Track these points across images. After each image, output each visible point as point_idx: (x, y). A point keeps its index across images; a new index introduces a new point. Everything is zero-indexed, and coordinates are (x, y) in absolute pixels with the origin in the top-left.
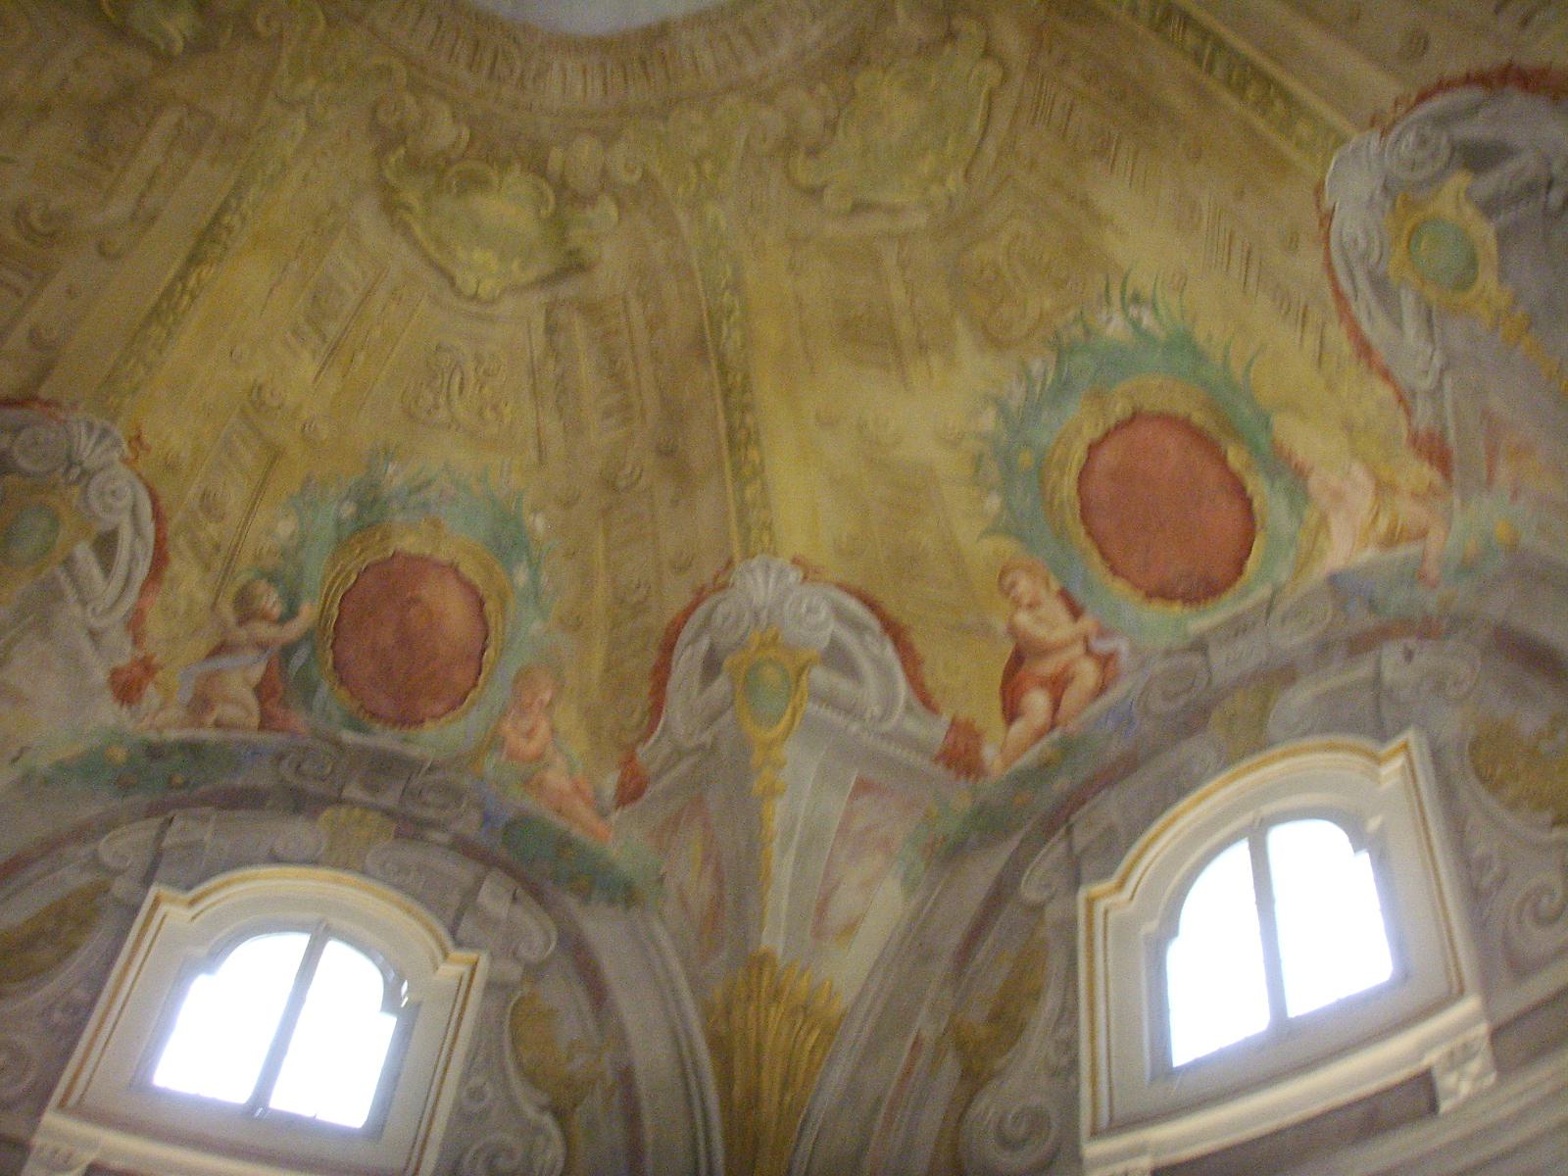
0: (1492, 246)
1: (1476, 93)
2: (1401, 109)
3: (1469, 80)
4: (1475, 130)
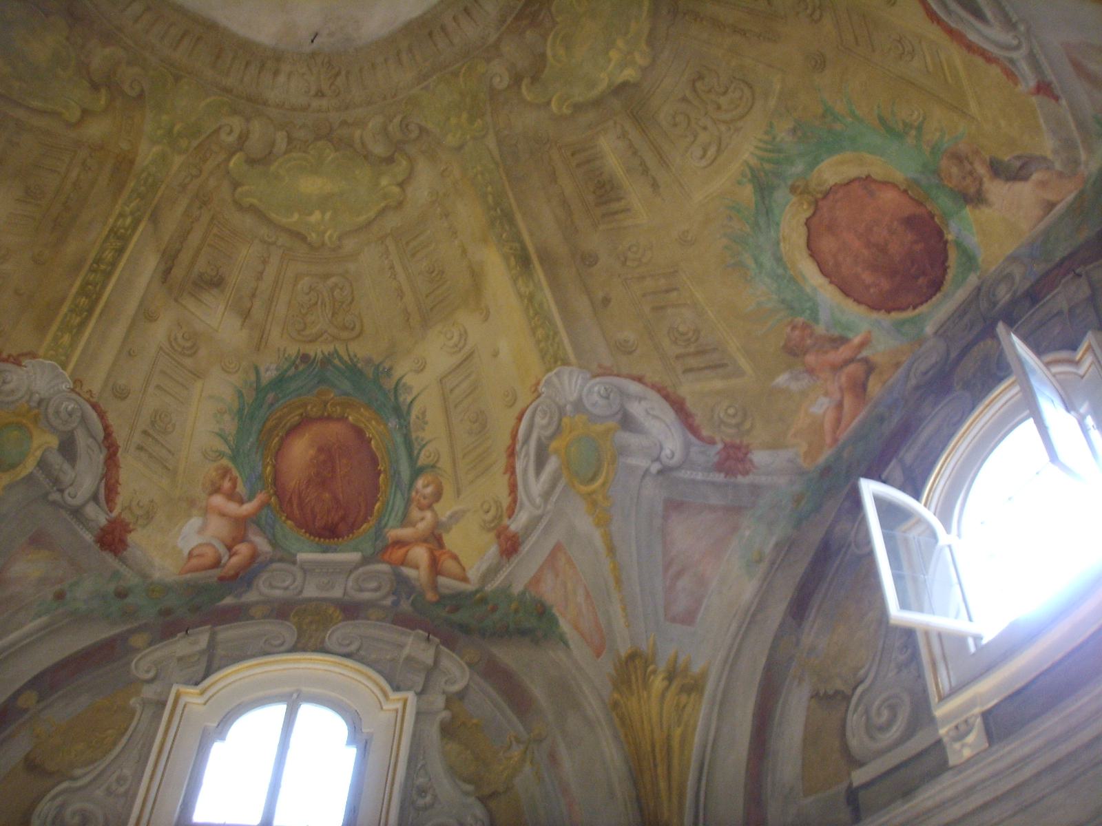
0: (24, 473)
1: (101, 435)
2: (87, 396)
3: (106, 428)
4: (82, 440)
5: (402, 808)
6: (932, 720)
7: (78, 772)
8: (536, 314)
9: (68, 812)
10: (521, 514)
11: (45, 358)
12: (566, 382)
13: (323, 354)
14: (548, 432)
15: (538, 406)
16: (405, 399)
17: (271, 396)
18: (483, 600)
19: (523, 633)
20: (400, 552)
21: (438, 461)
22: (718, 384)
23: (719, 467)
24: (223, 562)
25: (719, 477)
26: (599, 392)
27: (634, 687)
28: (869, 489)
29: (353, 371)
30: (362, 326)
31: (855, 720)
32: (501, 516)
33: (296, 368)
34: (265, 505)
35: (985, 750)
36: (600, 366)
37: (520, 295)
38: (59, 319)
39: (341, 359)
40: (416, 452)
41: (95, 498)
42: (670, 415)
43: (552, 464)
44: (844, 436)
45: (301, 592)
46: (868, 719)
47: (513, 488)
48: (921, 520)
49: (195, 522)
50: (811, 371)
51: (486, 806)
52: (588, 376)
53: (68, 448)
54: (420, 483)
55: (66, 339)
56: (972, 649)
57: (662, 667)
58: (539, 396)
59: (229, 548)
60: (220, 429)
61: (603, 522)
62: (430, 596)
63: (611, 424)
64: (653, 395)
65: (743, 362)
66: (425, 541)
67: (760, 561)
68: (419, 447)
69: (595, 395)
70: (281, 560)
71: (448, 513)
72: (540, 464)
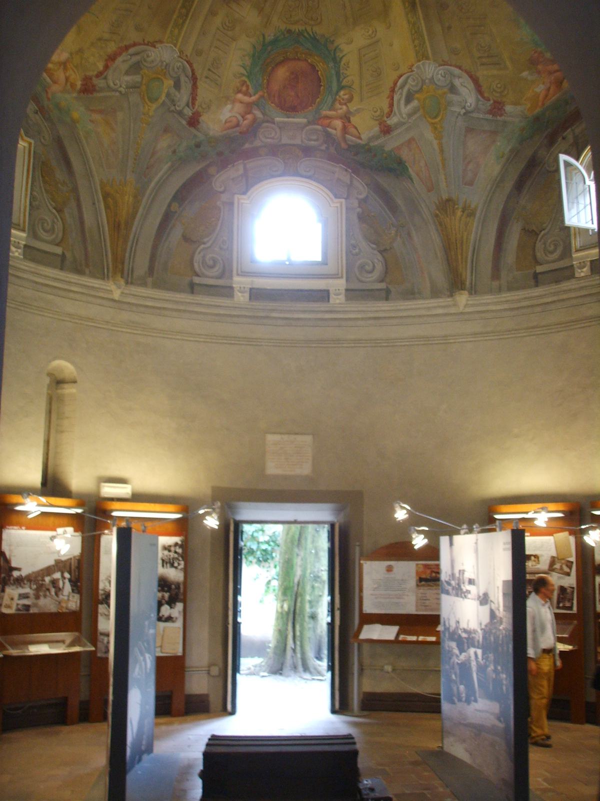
3: (193, 71)
4: (183, 79)
5: (347, 255)
6: (571, 256)
7: (205, 240)
8: (416, 32)
9: (208, 258)
10: (394, 118)
11: (168, 43)
12: (427, 69)
13: (299, 30)
14: (415, 89)
15: (411, 75)
16: (339, 56)
17: (269, 48)
18: (369, 150)
19: (390, 170)
20: (328, 121)
21: (352, 85)
22: (495, 72)
23: (490, 112)
24: (240, 123)
25: (490, 117)
26: (441, 74)
27: (448, 213)
28: (563, 157)
29: (314, 40)
30: (321, 19)
31: (539, 245)
32: (383, 116)
33: (284, 35)
34: (262, 97)
35: (589, 275)
36: (443, 61)
37: (409, 22)
38: (173, 20)
39: (308, 33)
40: (341, 79)
41: (188, 105)
42: (471, 86)
43: (415, 103)
44: (548, 103)
45: (280, 140)
46: (545, 246)
47: (391, 105)
48: (577, 168)
49: (229, 107)
50: (539, 73)
51: (382, 254)
52: (437, 65)
53: (177, 85)
54: (342, 93)
55: (176, 31)
56: (591, 233)
57: (461, 206)
58: (412, 71)
59: (243, 117)
60: (243, 64)
61: (439, 137)
62: (343, 145)
63: (445, 90)
64: (465, 76)
65: (508, 63)
66: (341, 118)
67: (502, 157)
68: (343, 77)
69: (440, 76)
70: (268, 121)
71: (355, 108)
72: (409, 100)
